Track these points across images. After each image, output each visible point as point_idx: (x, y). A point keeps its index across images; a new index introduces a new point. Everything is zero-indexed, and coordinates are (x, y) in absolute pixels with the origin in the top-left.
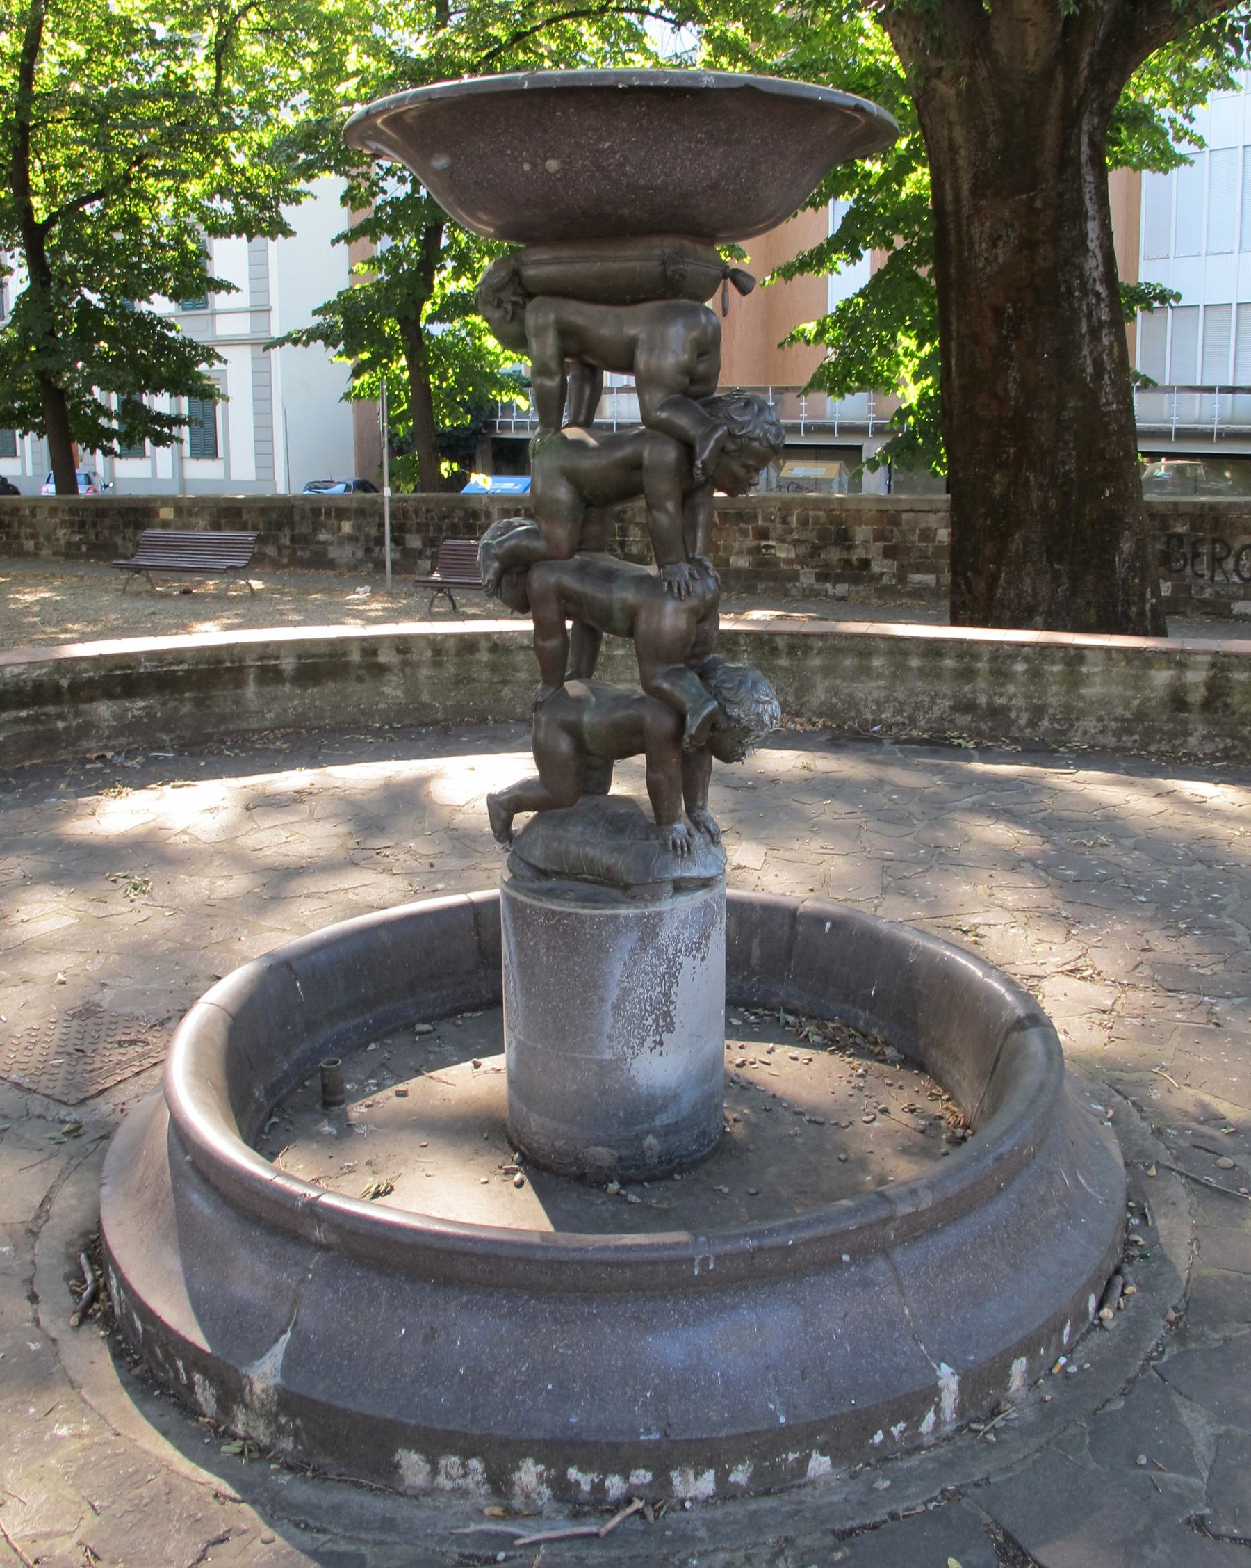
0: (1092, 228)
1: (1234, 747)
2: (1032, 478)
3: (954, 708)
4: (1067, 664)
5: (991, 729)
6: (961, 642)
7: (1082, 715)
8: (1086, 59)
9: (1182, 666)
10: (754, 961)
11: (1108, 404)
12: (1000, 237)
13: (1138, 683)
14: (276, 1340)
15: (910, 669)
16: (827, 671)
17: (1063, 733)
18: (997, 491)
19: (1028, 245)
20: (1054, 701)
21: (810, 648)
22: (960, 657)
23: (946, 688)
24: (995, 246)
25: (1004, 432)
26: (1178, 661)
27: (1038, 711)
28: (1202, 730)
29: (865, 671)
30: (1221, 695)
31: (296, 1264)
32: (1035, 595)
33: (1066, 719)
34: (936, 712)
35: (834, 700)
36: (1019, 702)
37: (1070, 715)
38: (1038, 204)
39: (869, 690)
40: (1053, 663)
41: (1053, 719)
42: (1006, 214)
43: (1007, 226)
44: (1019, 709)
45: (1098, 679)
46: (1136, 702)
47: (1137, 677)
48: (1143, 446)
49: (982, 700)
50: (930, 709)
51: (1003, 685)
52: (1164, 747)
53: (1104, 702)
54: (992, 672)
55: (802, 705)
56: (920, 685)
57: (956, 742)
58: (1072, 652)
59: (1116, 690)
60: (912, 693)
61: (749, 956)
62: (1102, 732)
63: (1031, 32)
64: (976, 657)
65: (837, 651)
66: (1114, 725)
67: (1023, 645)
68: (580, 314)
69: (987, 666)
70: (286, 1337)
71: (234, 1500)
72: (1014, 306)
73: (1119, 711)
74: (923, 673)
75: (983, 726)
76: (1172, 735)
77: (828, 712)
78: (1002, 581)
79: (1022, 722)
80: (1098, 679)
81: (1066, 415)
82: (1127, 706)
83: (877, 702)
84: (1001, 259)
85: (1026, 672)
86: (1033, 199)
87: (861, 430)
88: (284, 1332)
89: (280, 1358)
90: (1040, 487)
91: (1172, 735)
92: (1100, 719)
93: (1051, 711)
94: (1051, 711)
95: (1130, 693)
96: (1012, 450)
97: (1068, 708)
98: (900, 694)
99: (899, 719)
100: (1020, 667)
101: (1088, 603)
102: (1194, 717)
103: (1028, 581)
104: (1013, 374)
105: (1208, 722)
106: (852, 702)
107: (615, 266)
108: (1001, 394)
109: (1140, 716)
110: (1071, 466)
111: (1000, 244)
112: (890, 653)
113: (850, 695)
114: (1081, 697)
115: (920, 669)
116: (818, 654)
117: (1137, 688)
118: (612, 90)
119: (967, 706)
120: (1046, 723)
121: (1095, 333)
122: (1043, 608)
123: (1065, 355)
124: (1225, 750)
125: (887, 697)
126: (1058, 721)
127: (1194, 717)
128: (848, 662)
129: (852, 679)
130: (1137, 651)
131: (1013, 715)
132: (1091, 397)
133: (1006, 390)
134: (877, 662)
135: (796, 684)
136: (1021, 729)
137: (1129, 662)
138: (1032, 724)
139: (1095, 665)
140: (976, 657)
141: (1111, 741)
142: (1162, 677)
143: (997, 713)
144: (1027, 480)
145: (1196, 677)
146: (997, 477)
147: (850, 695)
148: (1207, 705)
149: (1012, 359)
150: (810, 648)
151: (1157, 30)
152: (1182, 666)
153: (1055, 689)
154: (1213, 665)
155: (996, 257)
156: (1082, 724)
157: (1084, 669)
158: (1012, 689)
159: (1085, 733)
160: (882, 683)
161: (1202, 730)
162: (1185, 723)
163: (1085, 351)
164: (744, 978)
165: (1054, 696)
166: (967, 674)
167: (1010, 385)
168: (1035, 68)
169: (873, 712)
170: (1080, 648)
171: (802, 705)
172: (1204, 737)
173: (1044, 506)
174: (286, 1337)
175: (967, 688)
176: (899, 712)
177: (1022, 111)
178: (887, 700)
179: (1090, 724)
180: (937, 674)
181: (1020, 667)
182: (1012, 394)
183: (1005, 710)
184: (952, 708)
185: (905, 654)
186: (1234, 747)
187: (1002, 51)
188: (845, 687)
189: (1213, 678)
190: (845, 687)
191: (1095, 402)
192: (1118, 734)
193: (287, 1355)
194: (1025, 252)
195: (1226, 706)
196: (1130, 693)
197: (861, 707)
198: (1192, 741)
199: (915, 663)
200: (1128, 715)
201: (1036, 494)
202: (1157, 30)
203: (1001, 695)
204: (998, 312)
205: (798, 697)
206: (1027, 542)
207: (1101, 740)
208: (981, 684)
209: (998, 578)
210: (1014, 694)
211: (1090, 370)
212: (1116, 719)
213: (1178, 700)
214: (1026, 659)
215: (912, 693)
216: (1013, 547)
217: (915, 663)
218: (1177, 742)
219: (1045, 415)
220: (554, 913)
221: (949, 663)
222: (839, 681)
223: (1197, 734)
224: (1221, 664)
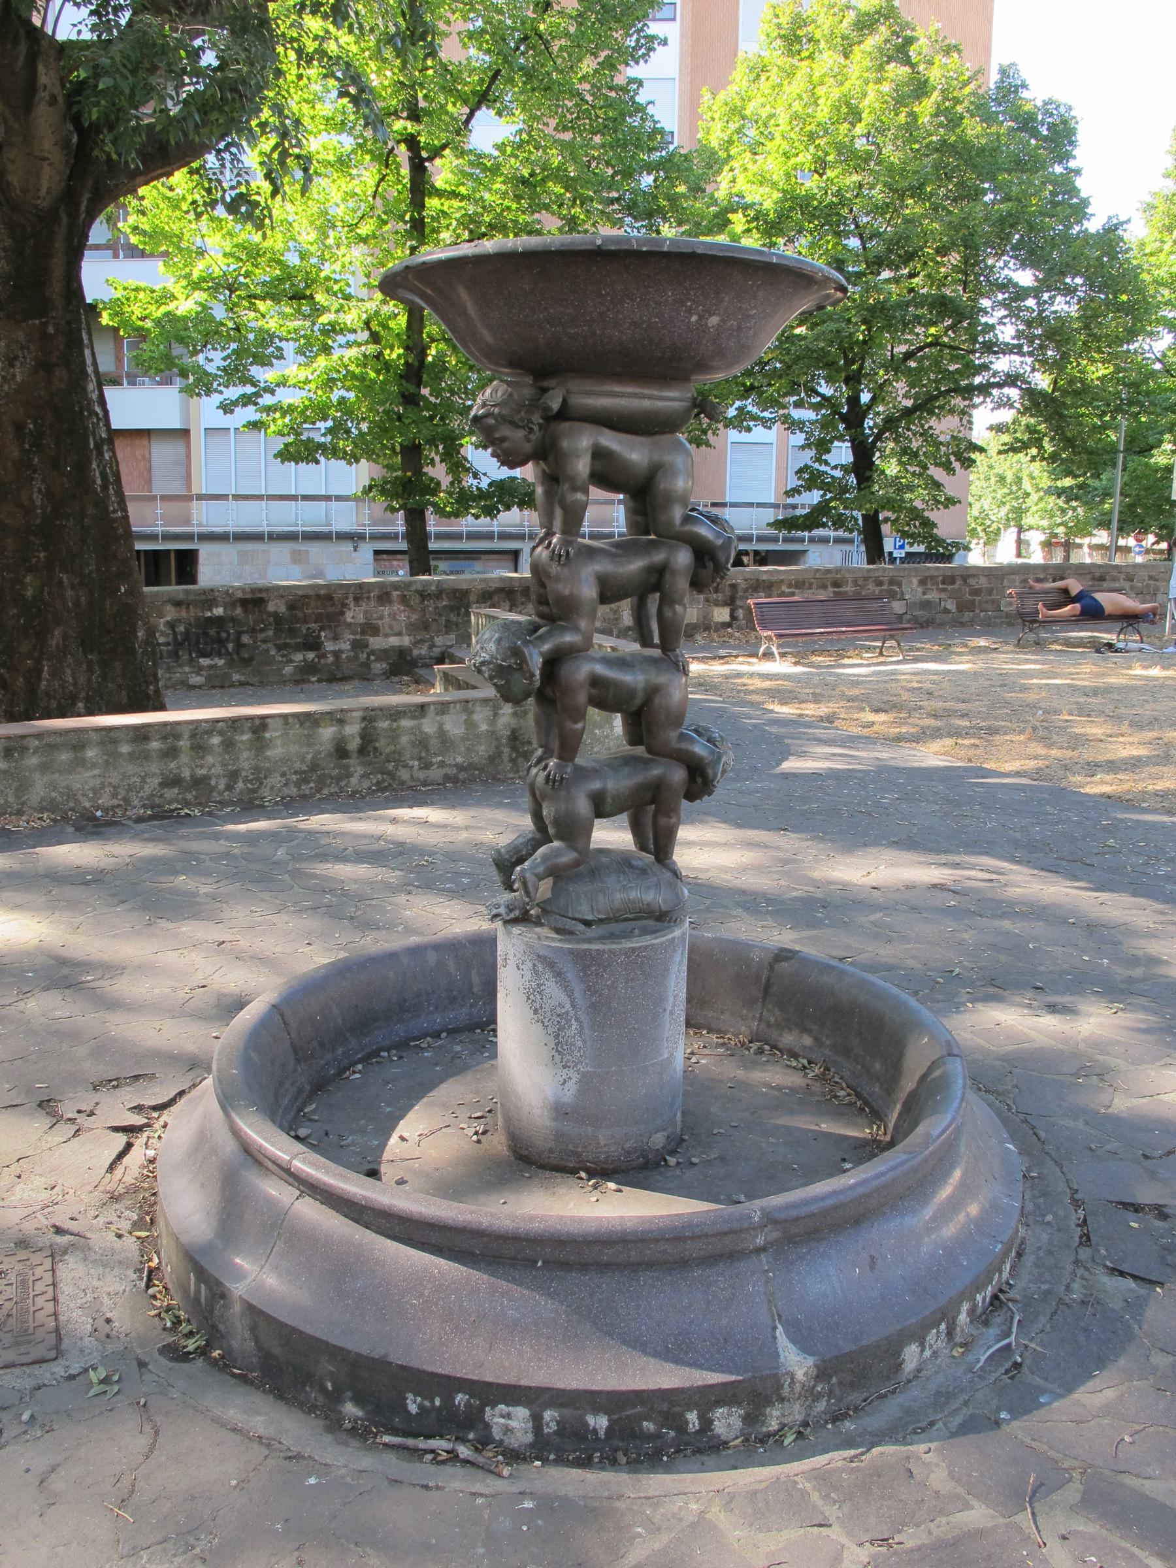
0: (87, 352)
1: (384, 780)
2: (65, 579)
3: (163, 785)
4: (254, 732)
5: (196, 798)
6: (165, 724)
7: (269, 773)
8: (85, 203)
9: (341, 722)
10: (476, 990)
11: (115, 511)
12: (16, 358)
13: (310, 740)
14: (775, 1338)
15: (121, 755)
16: (44, 768)
17: (254, 791)
18: (29, 593)
19: (44, 366)
20: (245, 765)
21: (27, 749)
22: (164, 738)
23: (154, 767)
24: (12, 366)
25: (32, 538)
26: (338, 718)
27: (233, 776)
28: (360, 770)
29: (80, 763)
30: (371, 741)
31: (753, 1273)
32: (75, 684)
33: (258, 779)
34: (148, 790)
35: (53, 794)
36: (218, 770)
37: (259, 776)
38: (51, 330)
39: (84, 780)
40: (242, 733)
41: (246, 780)
42: (21, 336)
43: (23, 348)
44: (218, 777)
45: (279, 742)
46: (310, 756)
47: (309, 736)
48: (403, 545)
49: (186, 774)
50: (142, 788)
51: (203, 758)
52: (334, 789)
53: (285, 760)
54: (192, 748)
55: (23, 803)
56: (131, 769)
57: (182, 813)
58: (257, 722)
59: (294, 748)
60: (124, 776)
61: (470, 986)
62: (286, 785)
63: (47, 170)
64: (177, 737)
65: (52, 748)
66: (294, 778)
67: (217, 721)
68: (610, 440)
69: (188, 744)
70: (780, 1329)
71: (863, 1454)
72: (35, 423)
73: (297, 765)
74: (132, 757)
75: (189, 796)
76: (339, 779)
77: (50, 806)
78: (45, 674)
79: (221, 787)
80: (279, 742)
81: (87, 521)
82: (303, 761)
83: (93, 790)
84: (19, 378)
85: (222, 743)
86: (45, 325)
87: (520, 537)
88: (775, 1328)
89: (790, 1346)
90: (73, 586)
91: (339, 779)
92: (283, 775)
93: (244, 774)
94: (244, 774)
95: (304, 750)
96: (42, 555)
97: (257, 769)
98: (114, 780)
99: (115, 802)
100: (216, 740)
101: (119, 686)
102: (353, 762)
103: (69, 671)
104: (38, 484)
105: (363, 764)
106: (70, 794)
107: (660, 404)
108: (26, 503)
109: (314, 767)
110: (92, 568)
111: (18, 364)
112: (102, 743)
113: (68, 787)
114: (267, 758)
115: (131, 754)
116: (35, 752)
117: (309, 745)
118: (637, 254)
119: (174, 781)
120: (240, 785)
121: (99, 447)
122: (83, 695)
123: (82, 468)
124: (378, 783)
125: (103, 784)
126: (250, 781)
127: (353, 762)
128: (64, 756)
129: (69, 772)
130: (308, 715)
131: (213, 783)
132: (101, 504)
133: (31, 500)
134: (90, 753)
135: (15, 784)
136: (220, 793)
137: (301, 724)
138: (229, 788)
139: (276, 730)
140: (177, 737)
141: (293, 791)
142: (327, 733)
143: (199, 783)
144: (61, 581)
145: (352, 729)
146: (28, 579)
147: (68, 787)
148: (362, 751)
149: (35, 471)
150: (27, 749)
151: (116, 185)
152: (341, 722)
153: (245, 755)
154: (364, 719)
155: (14, 376)
156: (269, 782)
157: (267, 735)
158: (210, 759)
159: (272, 788)
160: (96, 772)
161: (360, 770)
162: (347, 767)
163: (94, 466)
164: (472, 1006)
165: (245, 760)
166: (171, 753)
167: (35, 496)
168: (45, 204)
169: (90, 800)
170: (263, 718)
171: (23, 803)
172: (362, 776)
173: (77, 604)
174: (780, 1329)
175: (172, 765)
176: (114, 795)
177: (32, 242)
178: (103, 786)
179: (276, 780)
180: (146, 756)
181: (216, 740)
182: (38, 503)
183: (205, 779)
184: (160, 784)
185: (115, 742)
186: (384, 780)
187: (15, 183)
188: (63, 781)
189: (364, 729)
190: (63, 781)
191: (106, 508)
192: (298, 785)
193: (793, 1341)
194: (42, 373)
195: (376, 749)
196: (304, 750)
197: (79, 797)
198: (354, 780)
199: (125, 749)
200: (304, 768)
201: (69, 593)
202: (116, 185)
203: (202, 767)
204: (19, 427)
205: (18, 797)
206: (65, 636)
207: (286, 791)
208: (184, 759)
209: (40, 671)
210: (213, 765)
211: (99, 481)
212: (296, 773)
213: (340, 751)
214: (221, 733)
215: (124, 776)
216: (54, 643)
217: (125, 749)
218: (343, 784)
219: (72, 522)
220: (634, 950)
221: (155, 745)
222: (56, 776)
223: (358, 776)
224: (370, 716)
